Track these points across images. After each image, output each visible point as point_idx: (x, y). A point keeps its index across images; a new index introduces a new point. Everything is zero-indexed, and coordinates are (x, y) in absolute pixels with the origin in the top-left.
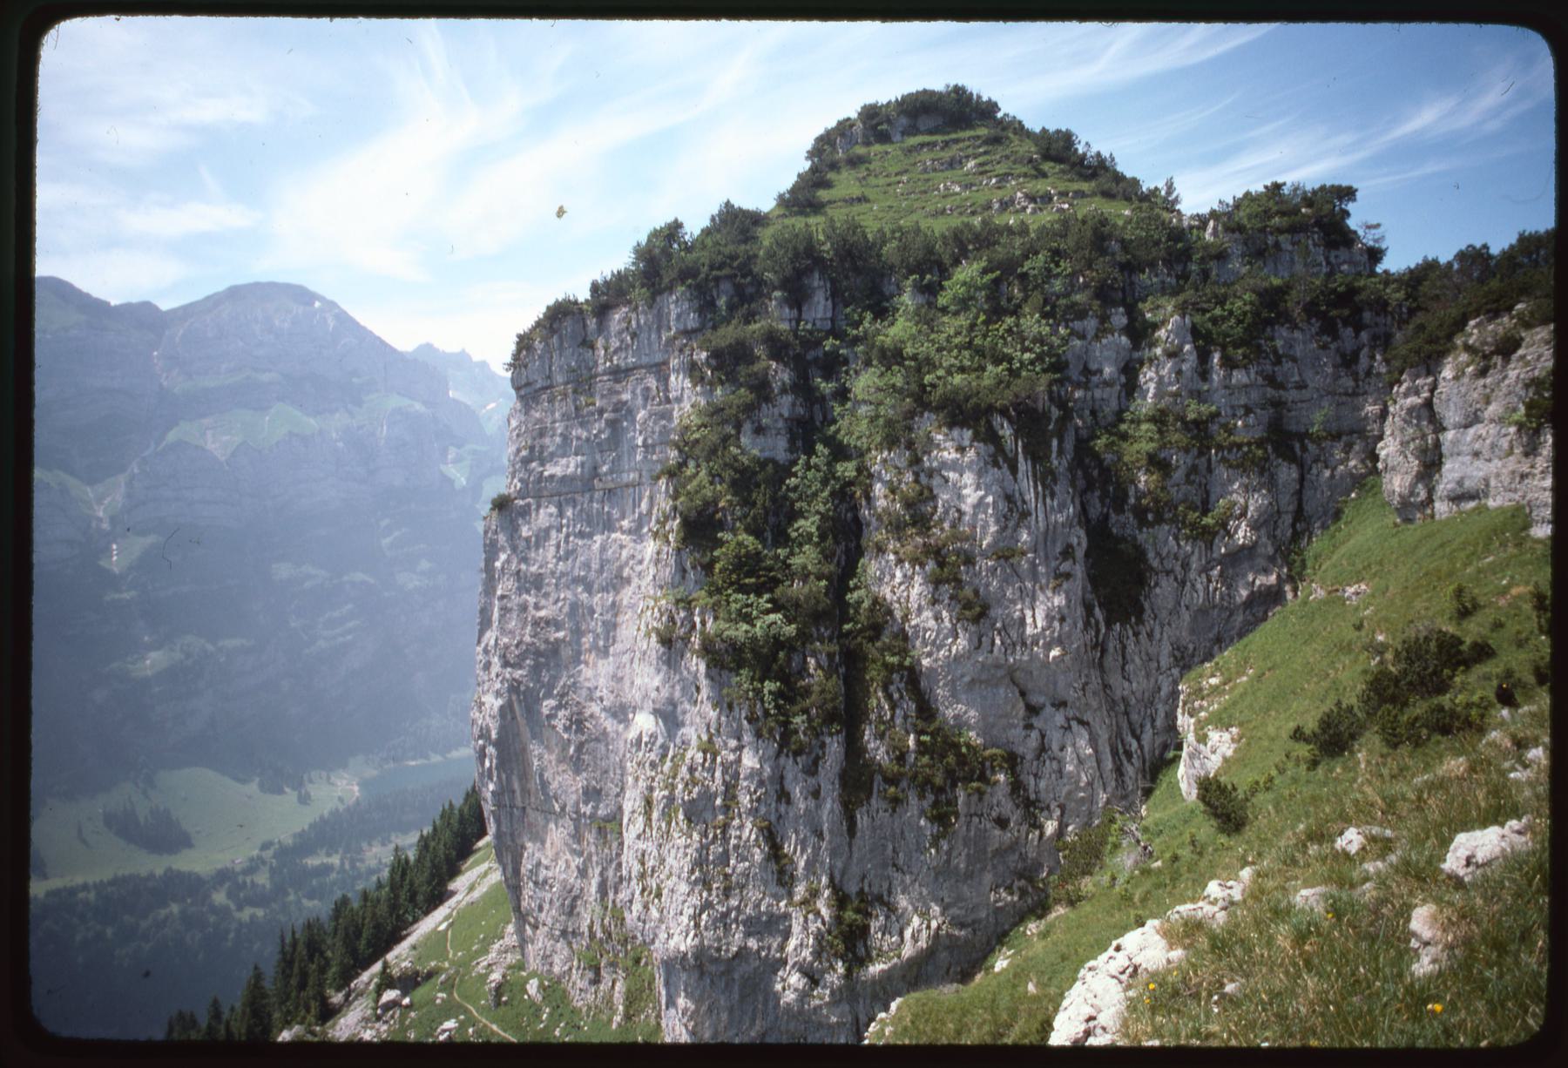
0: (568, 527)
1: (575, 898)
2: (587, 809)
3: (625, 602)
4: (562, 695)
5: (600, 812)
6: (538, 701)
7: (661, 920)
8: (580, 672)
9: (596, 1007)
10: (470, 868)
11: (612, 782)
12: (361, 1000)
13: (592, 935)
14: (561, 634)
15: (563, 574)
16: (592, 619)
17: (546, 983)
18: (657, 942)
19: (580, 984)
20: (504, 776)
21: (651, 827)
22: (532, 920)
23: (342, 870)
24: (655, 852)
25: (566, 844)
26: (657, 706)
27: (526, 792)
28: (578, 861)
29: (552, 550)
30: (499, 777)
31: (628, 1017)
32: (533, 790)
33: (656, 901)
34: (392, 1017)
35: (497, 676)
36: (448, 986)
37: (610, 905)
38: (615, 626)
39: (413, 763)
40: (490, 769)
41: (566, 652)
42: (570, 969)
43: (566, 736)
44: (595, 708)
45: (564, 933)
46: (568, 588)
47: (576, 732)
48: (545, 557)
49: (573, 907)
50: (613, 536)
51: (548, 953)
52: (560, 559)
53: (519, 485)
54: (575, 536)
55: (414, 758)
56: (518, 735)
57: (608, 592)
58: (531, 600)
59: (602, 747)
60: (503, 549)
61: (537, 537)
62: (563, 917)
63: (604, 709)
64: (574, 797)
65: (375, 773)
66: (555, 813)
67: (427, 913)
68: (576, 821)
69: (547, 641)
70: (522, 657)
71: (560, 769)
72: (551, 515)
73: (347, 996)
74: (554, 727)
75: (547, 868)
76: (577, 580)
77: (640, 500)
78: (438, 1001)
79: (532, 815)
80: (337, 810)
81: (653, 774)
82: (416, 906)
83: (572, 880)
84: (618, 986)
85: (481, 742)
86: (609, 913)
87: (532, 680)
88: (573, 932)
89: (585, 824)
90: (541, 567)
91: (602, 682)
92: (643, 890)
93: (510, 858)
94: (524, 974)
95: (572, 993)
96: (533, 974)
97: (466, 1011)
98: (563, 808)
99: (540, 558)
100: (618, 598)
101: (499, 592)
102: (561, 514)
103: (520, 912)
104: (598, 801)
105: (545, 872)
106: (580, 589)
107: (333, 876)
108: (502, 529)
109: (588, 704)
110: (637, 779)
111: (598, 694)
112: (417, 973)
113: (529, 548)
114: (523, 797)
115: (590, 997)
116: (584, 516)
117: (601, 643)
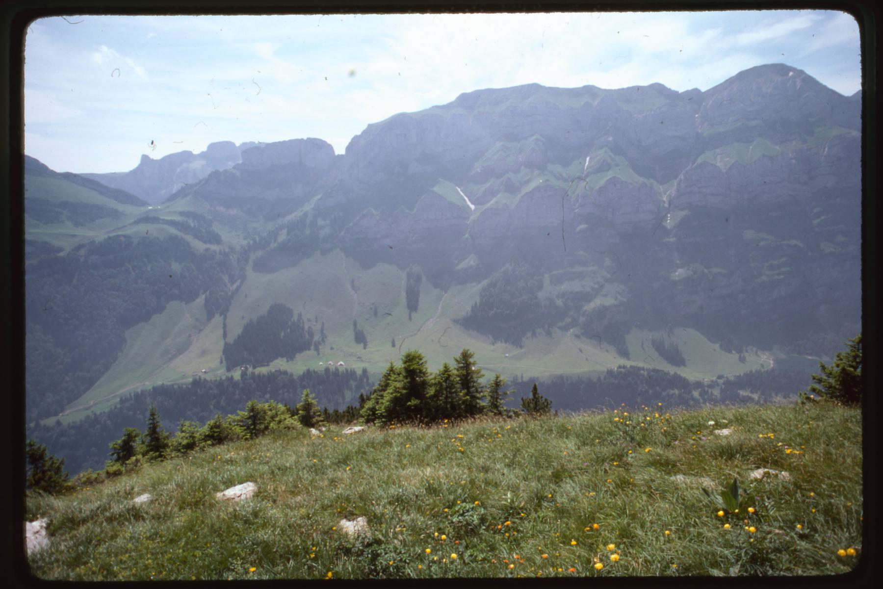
55: (811, 355)
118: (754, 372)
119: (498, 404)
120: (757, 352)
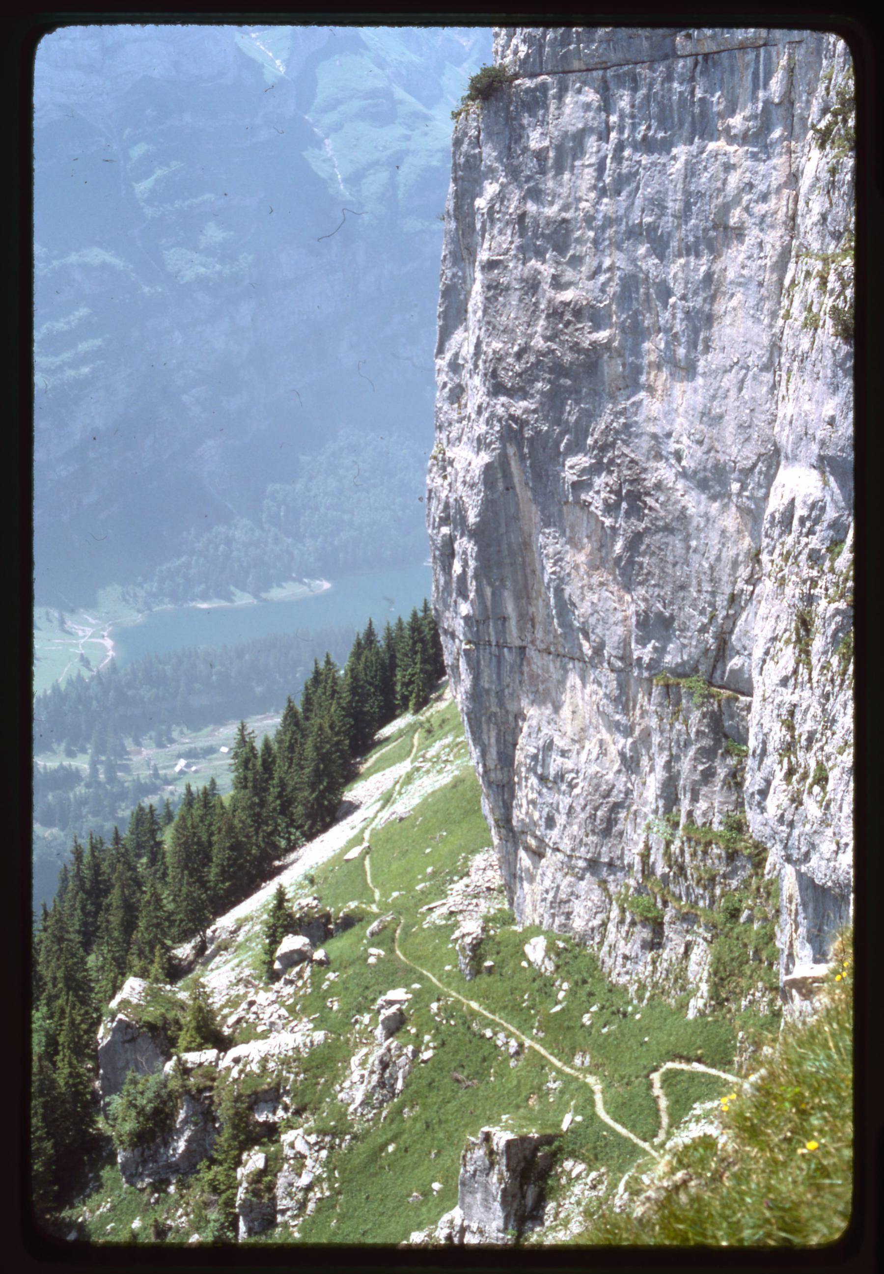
0: (621, 131)
1: (616, 807)
2: (645, 653)
3: (731, 275)
4: (604, 448)
5: (668, 658)
6: (557, 457)
7: (825, 822)
8: (638, 405)
9: (655, 985)
10: (377, 768)
11: (694, 606)
12: (225, 956)
13: (647, 870)
14: (602, 335)
15: (609, 221)
16: (665, 305)
17: (561, 945)
18: (815, 858)
19: (624, 948)
20: (488, 591)
21: (809, 663)
22: (533, 842)
23: (93, 782)
24: (816, 709)
25: (601, 713)
26: (830, 452)
27: (527, 620)
28: (624, 743)
29: (589, 174)
30: (479, 591)
31: (718, 1000)
32: (539, 618)
33: (816, 789)
34: (300, 975)
35: (479, 411)
36: (383, 937)
37: (683, 820)
38: (709, 320)
39: (205, 606)
40: (463, 577)
41: (612, 368)
42: (604, 924)
43: (608, 522)
44: (664, 472)
45: (593, 865)
46: (619, 248)
47: (628, 515)
48: (575, 188)
49: (611, 822)
50: (712, 146)
51: (563, 896)
52: (603, 192)
53: (523, 49)
54: (636, 148)
55: (204, 597)
56: (517, 518)
57: (698, 256)
58: (547, 270)
59: (676, 542)
60: (491, 173)
61: (559, 149)
62: (593, 839)
63: (683, 474)
64: (620, 630)
65: (139, 618)
66: (581, 659)
67: (310, 837)
68: (622, 676)
69: (576, 348)
70: (528, 376)
71: (595, 580)
72: (587, 107)
73: (200, 950)
74: (586, 505)
75: (564, 753)
76: (635, 233)
77: (768, 76)
78: (372, 960)
79: (538, 661)
80: (80, 677)
81: (814, 573)
82: (291, 823)
83: (610, 776)
84: (696, 954)
85: (445, 530)
86: (680, 832)
87: (546, 418)
88: (611, 865)
89: (640, 679)
90: (565, 208)
91: (680, 424)
92: (791, 772)
93: (493, 734)
94: (518, 929)
95: (609, 962)
96: (535, 930)
97: (421, 978)
98: (598, 650)
99: (564, 191)
100: (717, 267)
101: (483, 255)
102: (607, 106)
103: (511, 829)
104: (666, 640)
105: (560, 760)
106: (642, 250)
107: (81, 790)
108: (489, 136)
109: (653, 464)
110: (782, 582)
111: (672, 446)
112: (327, 917)
113: (543, 171)
114: (521, 630)
115: (643, 970)
116: (654, 109)
117: (681, 352)
118: (63, 687)
119: (535, 602)
120: (62, 622)
